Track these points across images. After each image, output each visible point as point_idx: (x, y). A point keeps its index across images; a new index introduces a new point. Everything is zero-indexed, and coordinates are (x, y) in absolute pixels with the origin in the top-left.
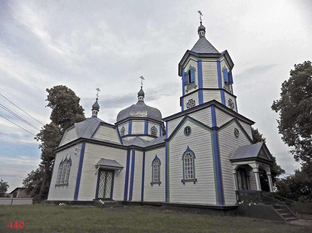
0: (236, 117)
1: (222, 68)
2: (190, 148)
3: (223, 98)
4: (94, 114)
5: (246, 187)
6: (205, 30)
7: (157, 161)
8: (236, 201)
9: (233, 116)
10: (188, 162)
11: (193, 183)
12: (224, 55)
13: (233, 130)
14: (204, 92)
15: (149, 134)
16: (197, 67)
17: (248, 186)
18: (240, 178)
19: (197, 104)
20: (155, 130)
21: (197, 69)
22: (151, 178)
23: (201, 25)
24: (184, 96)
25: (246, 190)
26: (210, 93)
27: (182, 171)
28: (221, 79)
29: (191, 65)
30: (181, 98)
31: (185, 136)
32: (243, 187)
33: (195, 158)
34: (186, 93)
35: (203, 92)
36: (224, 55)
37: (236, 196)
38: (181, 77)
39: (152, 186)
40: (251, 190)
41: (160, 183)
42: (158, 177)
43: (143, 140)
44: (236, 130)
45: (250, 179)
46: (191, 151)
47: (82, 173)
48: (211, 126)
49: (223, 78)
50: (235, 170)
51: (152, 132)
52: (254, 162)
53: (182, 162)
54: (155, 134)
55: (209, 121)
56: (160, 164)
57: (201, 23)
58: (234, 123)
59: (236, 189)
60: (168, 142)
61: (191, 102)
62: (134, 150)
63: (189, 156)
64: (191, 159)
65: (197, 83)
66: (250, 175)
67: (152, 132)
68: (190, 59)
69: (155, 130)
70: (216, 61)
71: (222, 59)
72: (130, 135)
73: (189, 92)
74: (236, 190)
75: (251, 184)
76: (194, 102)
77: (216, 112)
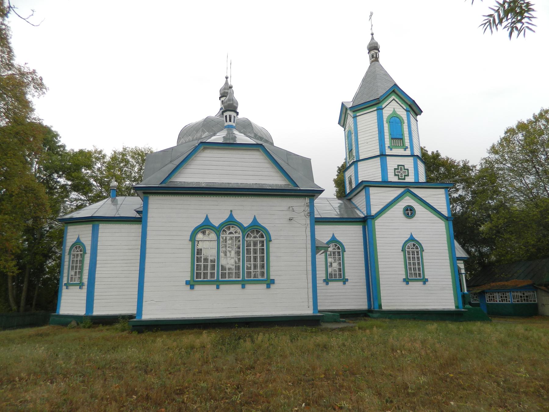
2: (414, 236)
4: (230, 121)
7: (79, 247)
33: (423, 251)
46: (417, 241)
47: (94, 306)
52: (462, 262)
64: (417, 252)
76: (399, 167)
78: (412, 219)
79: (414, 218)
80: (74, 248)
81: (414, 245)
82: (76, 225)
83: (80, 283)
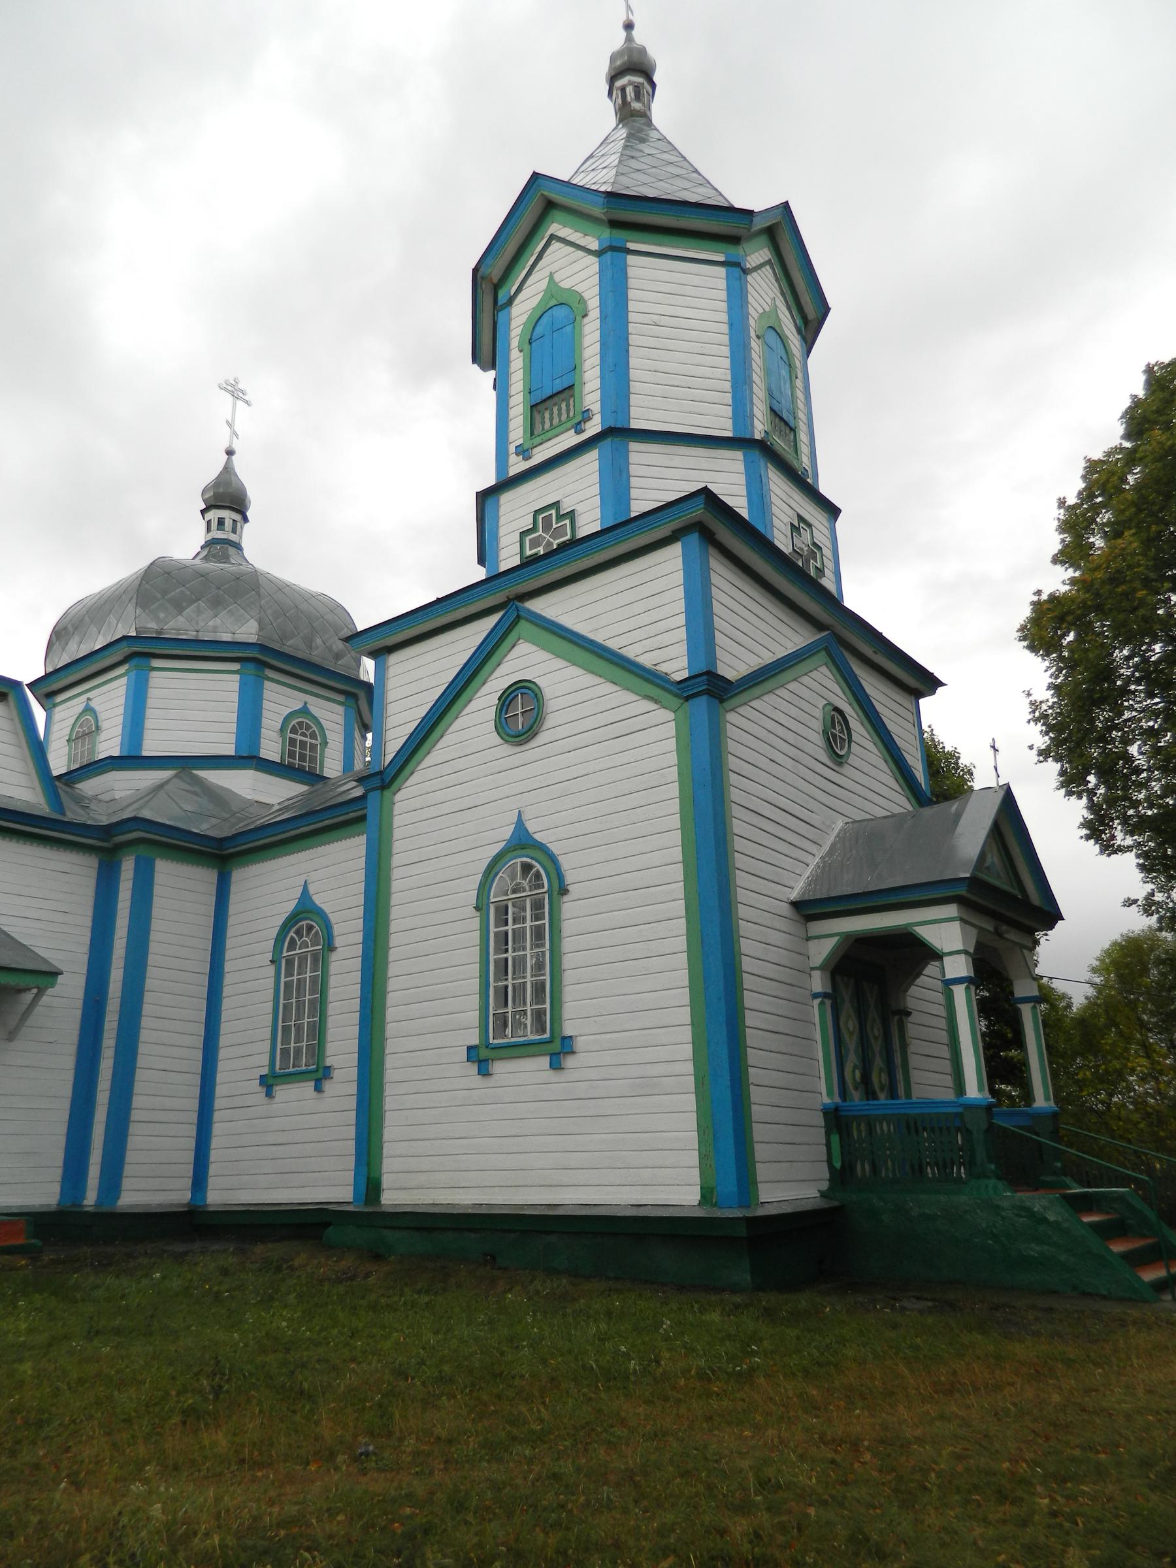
0: (834, 634)
1: (756, 316)
2: (531, 827)
3: (757, 492)
5: (884, 1078)
6: (656, 78)
7: (310, 928)
8: (827, 1176)
9: (818, 625)
10: (515, 922)
11: (545, 1061)
12: (771, 233)
13: (819, 713)
14: (640, 455)
15: (264, 754)
16: (597, 289)
17: (900, 1076)
18: (850, 1024)
19: (589, 524)
20: (313, 736)
21: (594, 304)
22: (267, 1045)
23: (629, 39)
24: (505, 484)
25: (883, 1099)
26: (677, 461)
27: (476, 988)
28: (748, 381)
29: (557, 277)
30: (485, 498)
31: (507, 749)
32: (866, 1079)
34: (517, 466)
35: (633, 458)
36: (771, 233)
37: (828, 1145)
38: (492, 374)
39: (269, 1094)
40: (914, 1100)
41: (320, 1075)
42: (311, 1036)
43: (217, 797)
44: (836, 715)
45: (912, 1030)
46: (541, 848)
48: (678, 667)
49: (757, 378)
50: (822, 968)
51: (292, 742)
52: (952, 910)
53: (476, 923)
54: (313, 759)
55: (667, 639)
56: (331, 948)
57: (629, 26)
58: (824, 669)
59: (830, 1093)
60: (387, 793)
61: (547, 522)
62: (143, 850)
63: (525, 883)
64: (538, 906)
65: (591, 394)
66: (911, 1003)
67: (292, 742)
68: (553, 237)
69: (313, 736)
70: (721, 258)
71: (758, 255)
72: (131, 760)
73: (541, 455)
74: (827, 1100)
75: (914, 1061)
76: (567, 522)
77: (714, 578)
78: (533, 744)
79: (542, 738)
80: (292, 934)
81: (526, 868)
82: (286, 855)
83: (317, 1071)
